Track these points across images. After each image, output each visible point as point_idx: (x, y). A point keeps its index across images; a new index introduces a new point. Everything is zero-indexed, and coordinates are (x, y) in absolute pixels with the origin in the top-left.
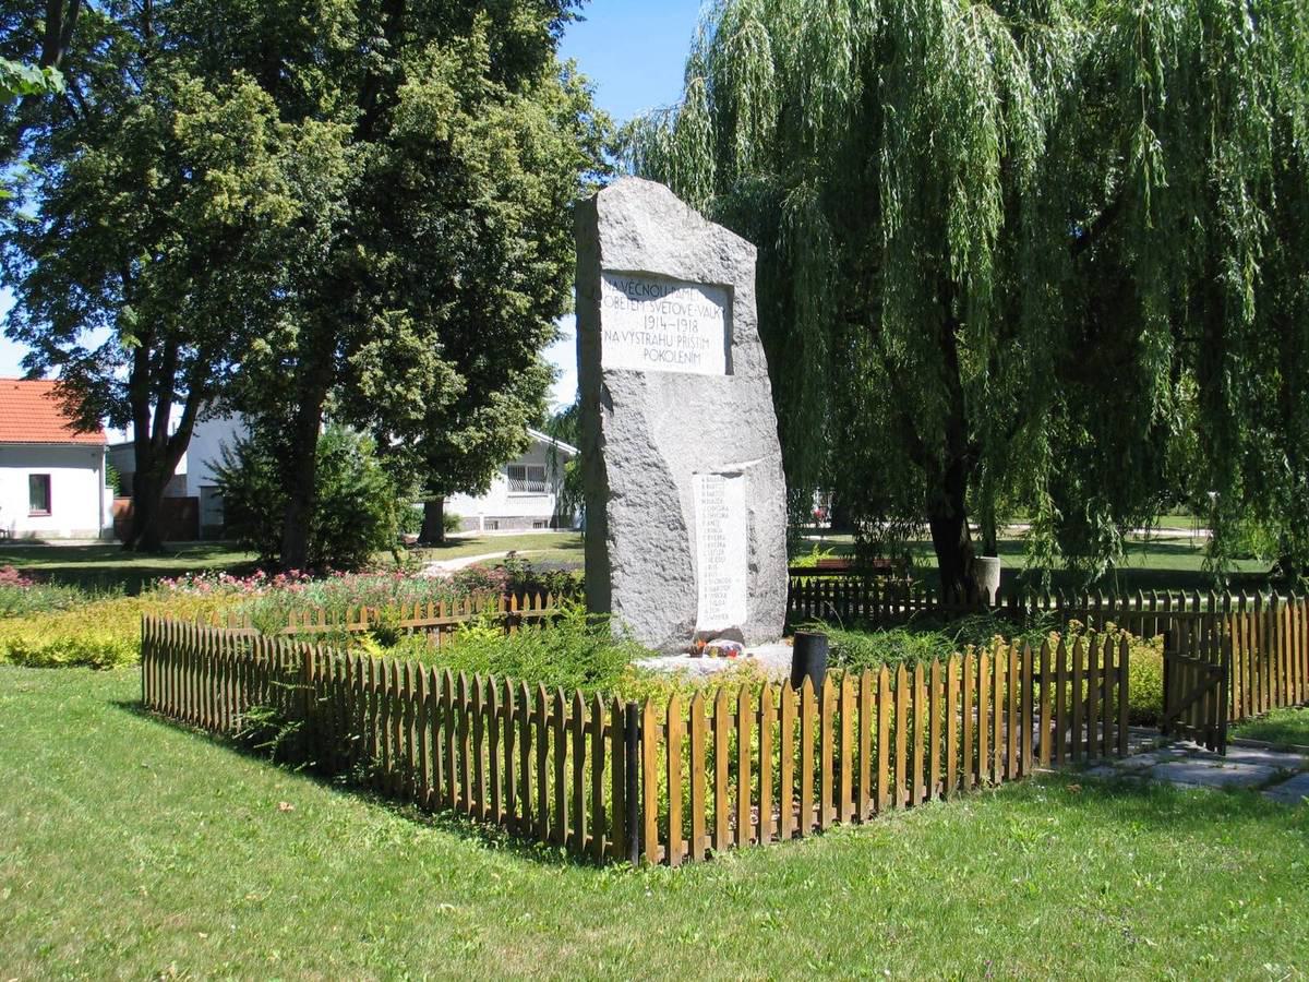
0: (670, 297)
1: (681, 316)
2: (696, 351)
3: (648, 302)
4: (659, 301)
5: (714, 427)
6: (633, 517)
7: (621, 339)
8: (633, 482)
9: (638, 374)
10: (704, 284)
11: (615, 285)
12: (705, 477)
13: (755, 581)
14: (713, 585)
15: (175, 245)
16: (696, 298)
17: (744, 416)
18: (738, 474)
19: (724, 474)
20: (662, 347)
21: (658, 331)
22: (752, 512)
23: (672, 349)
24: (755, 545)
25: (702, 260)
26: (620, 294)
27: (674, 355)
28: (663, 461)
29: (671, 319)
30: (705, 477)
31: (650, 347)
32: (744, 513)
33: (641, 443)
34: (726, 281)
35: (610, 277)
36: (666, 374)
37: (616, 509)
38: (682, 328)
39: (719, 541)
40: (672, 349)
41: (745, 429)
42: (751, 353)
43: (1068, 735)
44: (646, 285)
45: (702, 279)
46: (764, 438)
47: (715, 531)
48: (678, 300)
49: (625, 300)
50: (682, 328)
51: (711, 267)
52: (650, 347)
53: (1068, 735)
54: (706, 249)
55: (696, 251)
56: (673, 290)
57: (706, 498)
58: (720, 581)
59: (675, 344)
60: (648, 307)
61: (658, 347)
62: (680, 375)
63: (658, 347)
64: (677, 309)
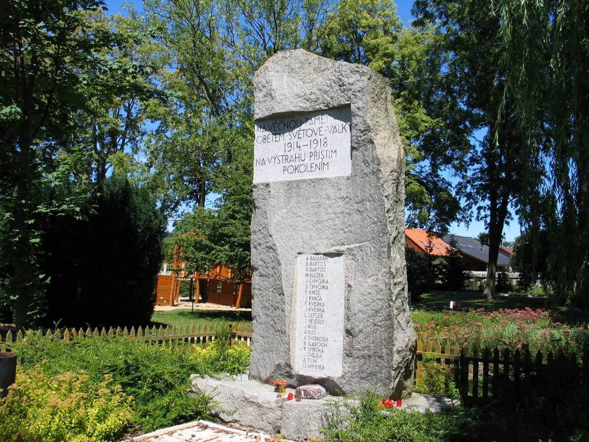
0: (304, 126)
1: (312, 138)
2: (325, 161)
3: (287, 134)
4: (295, 131)
5: (326, 217)
6: (262, 283)
7: (267, 163)
8: (261, 260)
9: (268, 185)
10: (330, 109)
11: (264, 128)
12: (309, 256)
13: (351, 345)
14: (312, 341)
15: (486, 11)
16: (328, 120)
17: (356, 206)
18: (339, 254)
19: (324, 254)
20: (297, 163)
21: (295, 152)
22: (349, 286)
23: (305, 163)
24: (349, 314)
25: (326, 92)
26: (267, 133)
27: (306, 166)
28: (275, 245)
29: (305, 141)
30: (309, 256)
31: (287, 165)
32: (343, 286)
33: (265, 233)
34: (343, 101)
35: (262, 124)
36: (291, 182)
37: (256, 280)
38: (314, 146)
39: (317, 307)
40: (305, 163)
41: (357, 217)
42: (367, 153)
43: (31, 222)
44: (283, 122)
45: (327, 106)
46: (375, 223)
47: (315, 298)
48: (311, 127)
49: (271, 136)
50: (314, 146)
51: (333, 95)
52: (287, 165)
53: (31, 222)
54: (328, 82)
55: (321, 87)
56: (307, 120)
57: (309, 272)
58: (317, 339)
59: (307, 158)
60: (287, 137)
61: (293, 164)
62: (304, 181)
63: (293, 164)
64: (309, 133)
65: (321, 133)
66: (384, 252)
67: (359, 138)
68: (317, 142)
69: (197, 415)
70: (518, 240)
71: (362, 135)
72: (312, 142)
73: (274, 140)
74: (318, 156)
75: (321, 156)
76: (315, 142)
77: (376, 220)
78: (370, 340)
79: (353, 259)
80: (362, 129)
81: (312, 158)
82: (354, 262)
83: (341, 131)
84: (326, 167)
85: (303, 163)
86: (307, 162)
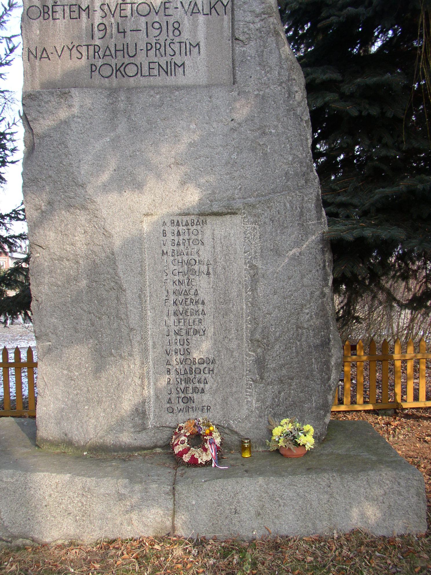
65: (169, 12)
66: (309, 210)
67: (252, 26)
68: (161, 28)
69: (164, 446)
70: (399, 226)
71: (257, 20)
72: (149, 25)
73: (67, 15)
74: (162, 50)
75: (169, 51)
76: (157, 26)
77: (290, 159)
78: (292, 353)
79: (255, 222)
80: (258, 11)
81: (152, 52)
82: (257, 227)
83: (206, 11)
84: (181, 70)
85: (132, 60)
86: (141, 58)
